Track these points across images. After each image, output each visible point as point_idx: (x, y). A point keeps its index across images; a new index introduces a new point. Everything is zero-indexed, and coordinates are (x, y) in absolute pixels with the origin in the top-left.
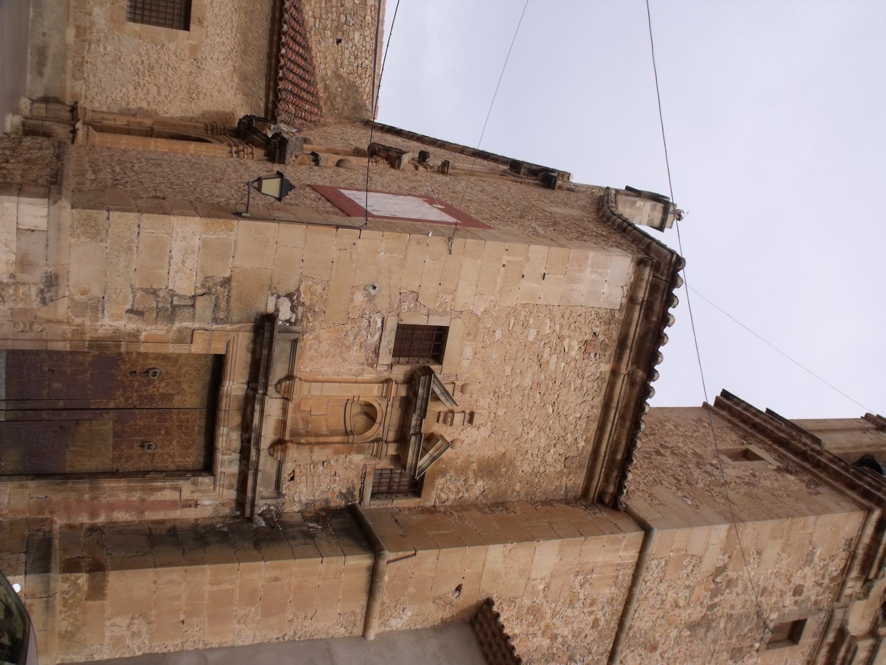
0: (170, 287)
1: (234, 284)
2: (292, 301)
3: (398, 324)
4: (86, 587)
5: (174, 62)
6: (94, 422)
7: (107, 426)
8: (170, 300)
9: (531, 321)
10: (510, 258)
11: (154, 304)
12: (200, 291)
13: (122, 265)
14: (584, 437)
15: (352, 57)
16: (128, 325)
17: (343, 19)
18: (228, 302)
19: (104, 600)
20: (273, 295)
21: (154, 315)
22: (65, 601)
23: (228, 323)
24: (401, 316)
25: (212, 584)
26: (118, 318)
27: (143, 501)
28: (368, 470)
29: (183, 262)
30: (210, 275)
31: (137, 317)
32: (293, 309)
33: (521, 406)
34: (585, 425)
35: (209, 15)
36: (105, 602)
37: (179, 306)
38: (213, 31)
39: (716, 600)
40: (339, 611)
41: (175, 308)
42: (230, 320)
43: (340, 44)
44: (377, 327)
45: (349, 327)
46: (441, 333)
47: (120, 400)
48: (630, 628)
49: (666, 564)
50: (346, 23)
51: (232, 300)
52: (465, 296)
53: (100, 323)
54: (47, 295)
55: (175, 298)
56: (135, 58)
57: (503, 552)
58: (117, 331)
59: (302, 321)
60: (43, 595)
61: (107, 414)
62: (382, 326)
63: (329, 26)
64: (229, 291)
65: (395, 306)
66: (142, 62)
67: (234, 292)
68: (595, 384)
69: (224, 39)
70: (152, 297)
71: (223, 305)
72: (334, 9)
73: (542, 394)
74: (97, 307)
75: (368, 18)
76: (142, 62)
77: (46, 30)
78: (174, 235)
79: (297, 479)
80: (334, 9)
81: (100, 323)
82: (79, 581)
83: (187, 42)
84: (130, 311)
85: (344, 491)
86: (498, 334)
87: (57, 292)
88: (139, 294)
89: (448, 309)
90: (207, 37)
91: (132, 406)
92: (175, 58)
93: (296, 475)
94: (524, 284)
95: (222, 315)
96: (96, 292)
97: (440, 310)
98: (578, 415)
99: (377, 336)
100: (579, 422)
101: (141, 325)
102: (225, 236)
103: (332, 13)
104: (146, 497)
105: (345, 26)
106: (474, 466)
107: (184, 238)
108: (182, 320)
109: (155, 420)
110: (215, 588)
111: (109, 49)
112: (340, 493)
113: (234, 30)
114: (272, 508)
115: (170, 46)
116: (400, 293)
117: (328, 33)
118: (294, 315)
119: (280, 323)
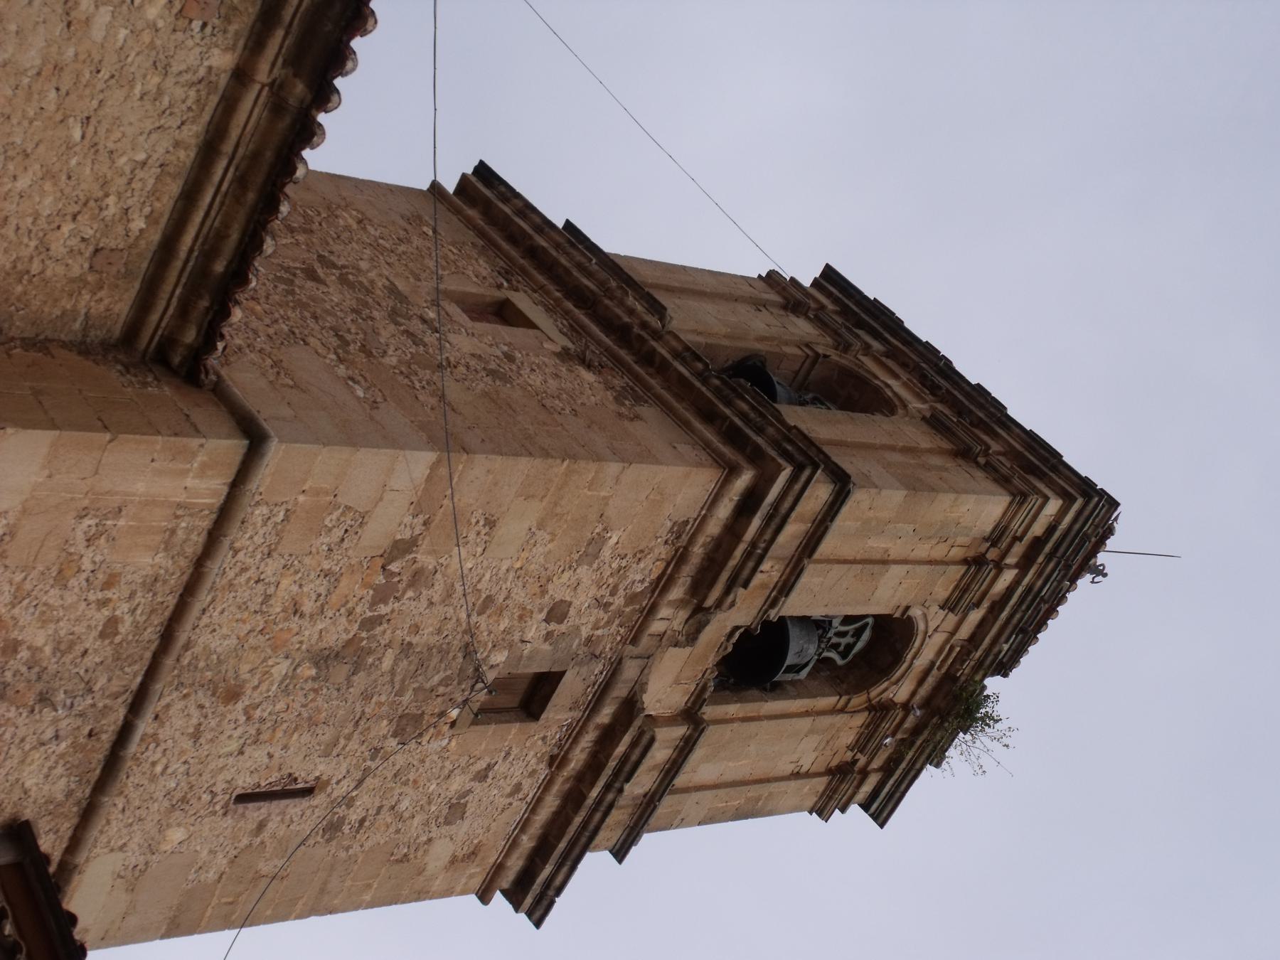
14: (147, 210)
34: (152, 181)
39: (383, 609)
48: (187, 647)
49: (286, 518)
68: (192, 93)
98: (141, 156)
100: (140, 174)
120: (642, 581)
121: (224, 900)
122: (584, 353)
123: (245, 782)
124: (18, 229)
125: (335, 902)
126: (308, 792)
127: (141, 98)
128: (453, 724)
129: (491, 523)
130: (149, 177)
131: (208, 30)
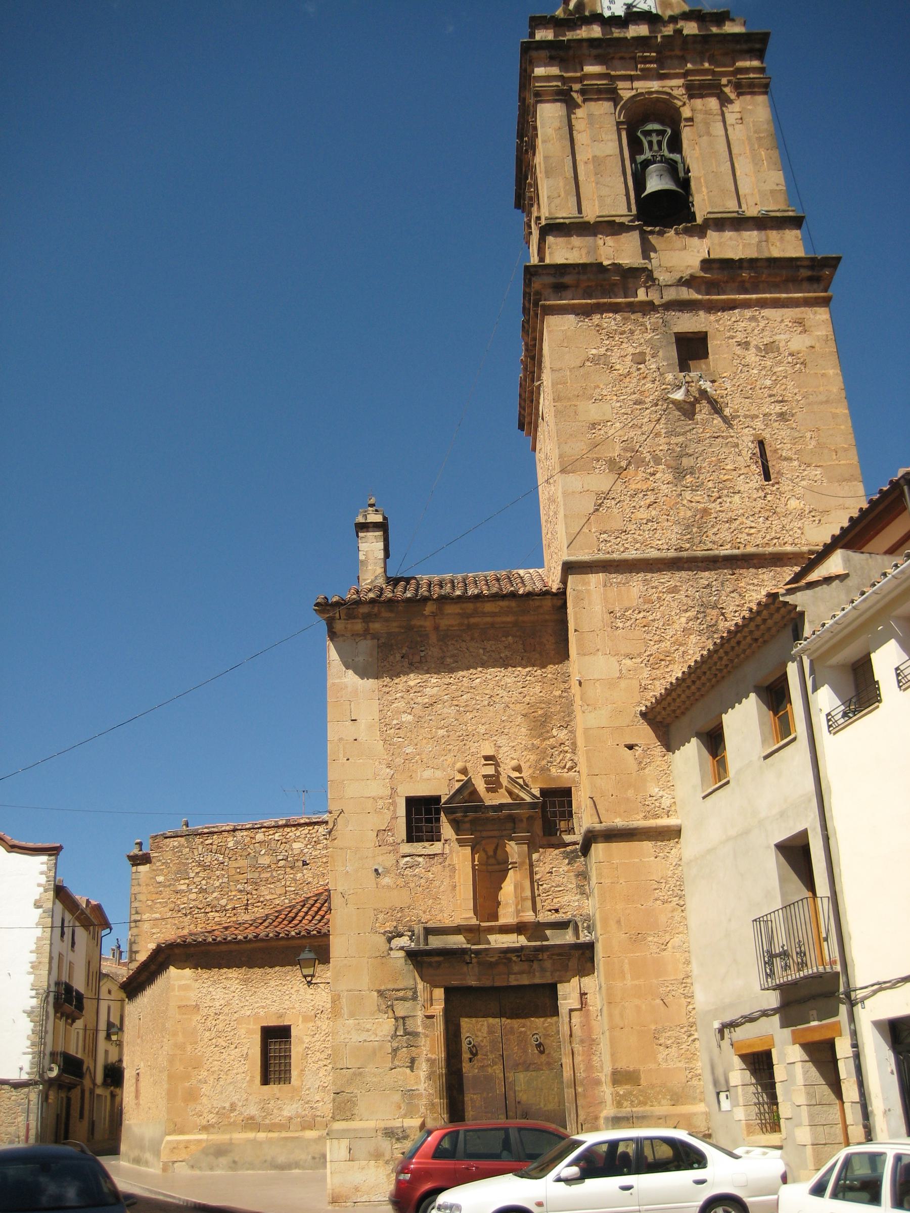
0: (389, 1038)
1: (383, 988)
2: (394, 937)
3: (408, 842)
4: (628, 1087)
5: (322, 1035)
6: (517, 1088)
7: (522, 1078)
8: (400, 1038)
9: (395, 722)
10: (341, 756)
11: (404, 1049)
12: (391, 1013)
13: (375, 1080)
14: (504, 639)
15: (318, 847)
16: (423, 1069)
17: (282, 863)
18: (398, 990)
19: (640, 1070)
20: (389, 954)
21: (413, 1048)
22: (641, 1103)
23: (416, 988)
24: (399, 841)
25: (623, 977)
26: (418, 1077)
27: (582, 1041)
28: (545, 843)
29: (368, 1031)
30: (376, 1008)
31: (416, 1062)
32: (400, 935)
33: (475, 711)
34: (490, 642)
35: (274, 1009)
36: (642, 1069)
37: (405, 1029)
38: (287, 1002)
39: (648, 457)
40: (653, 858)
41: (406, 1033)
42: (413, 986)
43: (308, 862)
44: (411, 860)
45: (412, 885)
46: (413, 803)
47: (497, 1070)
48: (680, 549)
49: (605, 532)
50: (286, 860)
51: (396, 987)
52: (378, 788)
53: (424, 1092)
54: (401, 1135)
55: (398, 1034)
56: (322, 1073)
57: (590, 712)
58: (429, 1078)
59: (410, 927)
60: (631, 1122)
61: (508, 1078)
62: (410, 856)
63: (292, 876)
64: (389, 990)
65: (391, 848)
66: (325, 1065)
67: (390, 986)
68: (449, 643)
69: (292, 991)
70: (399, 1053)
71: (401, 994)
72: (274, 874)
73: (462, 693)
74: (410, 1095)
75: (277, 836)
76: (325, 1065)
77: (310, 1157)
78: (347, 1040)
79: (557, 906)
80: (274, 874)
81: (424, 1092)
82: (621, 1093)
83: (301, 1026)
84: (412, 1068)
85: (567, 861)
86: (409, 750)
87: (397, 1128)
88: (397, 1063)
89: (391, 801)
90: (294, 1008)
91: (501, 1058)
92: (317, 1036)
93: (552, 908)
94: (362, 737)
95: (410, 994)
96: (397, 1097)
97: (392, 808)
98: (481, 651)
99: (420, 859)
100: (489, 648)
101: (423, 1059)
102: (344, 1000)
103: (279, 874)
104: (578, 1039)
105: (289, 859)
106: (537, 742)
107: (349, 1032)
108: (417, 1026)
109: (512, 1037)
110: (628, 976)
111: (317, 1098)
112: (568, 864)
113: (284, 983)
114: (585, 925)
115: (307, 1041)
116: (380, 846)
117: (299, 875)
118: (406, 933)
119: (413, 945)
120: (615, 319)
121: (834, 457)
122: (722, 105)
123: (757, 480)
124: (523, 687)
125: (835, 391)
126: (761, 443)
127: (457, 662)
128: (713, 382)
129: (593, 425)
130: (489, 645)
131: (423, 649)
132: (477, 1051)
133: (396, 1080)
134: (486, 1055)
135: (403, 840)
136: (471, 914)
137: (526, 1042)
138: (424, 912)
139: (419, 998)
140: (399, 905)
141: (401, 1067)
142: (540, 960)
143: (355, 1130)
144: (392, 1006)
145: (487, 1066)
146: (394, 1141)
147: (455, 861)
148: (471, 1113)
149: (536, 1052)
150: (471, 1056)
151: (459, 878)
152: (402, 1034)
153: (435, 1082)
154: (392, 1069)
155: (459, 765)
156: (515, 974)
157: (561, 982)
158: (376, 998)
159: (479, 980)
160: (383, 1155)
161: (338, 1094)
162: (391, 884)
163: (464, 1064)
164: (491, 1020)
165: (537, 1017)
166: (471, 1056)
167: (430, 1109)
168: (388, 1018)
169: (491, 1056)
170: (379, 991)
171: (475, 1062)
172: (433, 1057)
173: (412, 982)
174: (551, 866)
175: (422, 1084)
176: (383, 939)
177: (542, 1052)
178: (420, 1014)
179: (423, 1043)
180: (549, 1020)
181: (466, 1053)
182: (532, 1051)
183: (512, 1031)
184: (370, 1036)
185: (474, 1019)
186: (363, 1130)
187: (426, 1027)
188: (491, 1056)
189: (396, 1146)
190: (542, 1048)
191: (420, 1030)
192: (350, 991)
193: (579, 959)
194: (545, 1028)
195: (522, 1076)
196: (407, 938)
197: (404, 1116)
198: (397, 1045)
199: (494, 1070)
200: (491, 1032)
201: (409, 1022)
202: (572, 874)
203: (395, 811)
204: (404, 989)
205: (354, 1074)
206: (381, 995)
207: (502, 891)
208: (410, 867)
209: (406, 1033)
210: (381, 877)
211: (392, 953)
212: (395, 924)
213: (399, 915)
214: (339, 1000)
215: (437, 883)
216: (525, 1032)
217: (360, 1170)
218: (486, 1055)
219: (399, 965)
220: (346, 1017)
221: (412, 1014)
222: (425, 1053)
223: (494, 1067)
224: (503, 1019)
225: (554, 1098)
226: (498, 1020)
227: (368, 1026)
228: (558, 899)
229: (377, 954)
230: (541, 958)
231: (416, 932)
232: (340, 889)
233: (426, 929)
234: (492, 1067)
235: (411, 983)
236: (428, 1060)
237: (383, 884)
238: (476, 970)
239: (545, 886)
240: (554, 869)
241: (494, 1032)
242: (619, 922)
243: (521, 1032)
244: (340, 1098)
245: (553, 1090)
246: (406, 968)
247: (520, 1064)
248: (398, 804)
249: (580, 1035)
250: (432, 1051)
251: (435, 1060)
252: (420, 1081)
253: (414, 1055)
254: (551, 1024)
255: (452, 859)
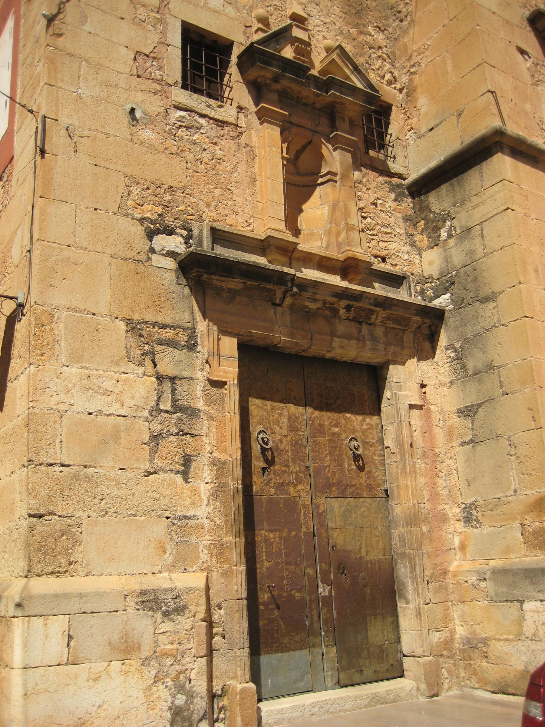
0: (146, 413)
1: (136, 316)
2: (158, 232)
8: (166, 415)
11: (172, 438)
18: (163, 327)
20: (149, 259)
21: (188, 438)
23: (194, 328)
26: (196, 492)
29: (107, 393)
30: (124, 353)
31: (194, 464)
32: (170, 232)
37: (174, 401)
41: (177, 408)
42: (189, 325)
55: (162, 407)
59: (186, 221)
62: (186, 110)
64: (147, 323)
65: (158, 87)
67: (150, 317)
70: (163, 443)
71: (168, 334)
78: (62, 407)
81: (206, 522)
84: (185, 475)
85: (393, 196)
87: (166, 590)
89: (158, 16)
93: (379, 253)
95: (183, 337)
97: (160, 28)
99: (203, 121)
102: (61, 326)
107: (68, 391)
108: (193, 396)
109: (322, 440)
112: (395, 200)
114: (418, 288)
116: (139, 76)
118: (178, 230)
132: (273, 457)
133: (157, 496)
134: (287, 466)
135: (176, 83)
136: (282, 226)
137: (340, 451)
138: (208, 205)
139: (199, 348)
140: (168, 182)
141: (166, 471)
142: (370, 324)
143: (81, 595)
144: (152, 353)
145: (288, 484)
146: (159, 616)
147: (255, 142)
148: (266, 564)
149: (354, 467)
150: (265, 466)
151: (260, 169)
152: (169, 408)
153: (224, 504)
154: (148, 474)
155: (261, 11)
156: (339, 337)
157: (395, 362)
158: (124, 333)
159: (292, 335)
160: (139, 648)
161: (41, 516)
162: (157, 143)
163: (254, 478)
164: (292, 408)
165: (353, 413)
166: (265, 466)
167: (217, 555)
168: (144, 374)
169: (294, 468)
170: (129, 322)
171: (272, 476)
172: (223, 457)
173: (187, 317)
174: (376, 195)
175: (204, 506)
176: (139, 230)
177: (361, 469)
178: (200, 376)
179: (204, 431)
180: (368, 420)
181: (257, 458)
182: (349, 464)
183: (320, 430)
184: (109, 404)
185: (268, 403)
186: (99, 595)
187: (209, 401)
188: (294, 468)
189: (164, 627)
190: (361, 462)
191: (200, 405)
192: (75, 310)
193: (414, 335)
194: (364, 432)
195: (336, 505)
196: (181, 239)
197: (171, 568)
198: (159, 427)
199: (299, 491)
200: (293, 428)
201: (182, 388)
202: (399, 215)
203: (163, 33)
204: (175, 327)
205: (76, 477)
206: (133, 328)
207: (302, 214)
208: (187, 128)
209: (177, 408)
210: (139, 127)
211: (154, 257)
212: (160, 210)
213: (168, 197)
214: (50, 324)
215: (227, 166)
216: (339, 435)
217: (91, 683)
218: (287, 466)
219: (165, 282)
220: (63, 359)
221: (186, 374)
222: (208, 448)
223: (299, 487)
224: (310, 410)
225: (378, 542)
226: (301, 409)
227: (108, 385)
228: (385, 244)
229: (128, 254)
230: (373, 320)
231: (195, 232)
232: (65, 120)
233: (214, 230)
234: (295, 486)
235: (184, 318)
236: (214, 462)
237: (141, 138)
238: (287, 318)
239: (368, 220)
240: (379, 201)
241: (297, 430)
242: (536, 271)
243: (334, 434)
244: (41, 525)
245: (377, 528)
246: (178, 289)
247: (333, 484)
248: (170, 27)
249: (422, 445)
250: (220, 445)
251: (225, 463)
252: (201, 500)
253: (189, 451)
254: (371, 427)
255: (249, 136)
